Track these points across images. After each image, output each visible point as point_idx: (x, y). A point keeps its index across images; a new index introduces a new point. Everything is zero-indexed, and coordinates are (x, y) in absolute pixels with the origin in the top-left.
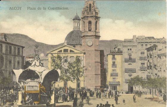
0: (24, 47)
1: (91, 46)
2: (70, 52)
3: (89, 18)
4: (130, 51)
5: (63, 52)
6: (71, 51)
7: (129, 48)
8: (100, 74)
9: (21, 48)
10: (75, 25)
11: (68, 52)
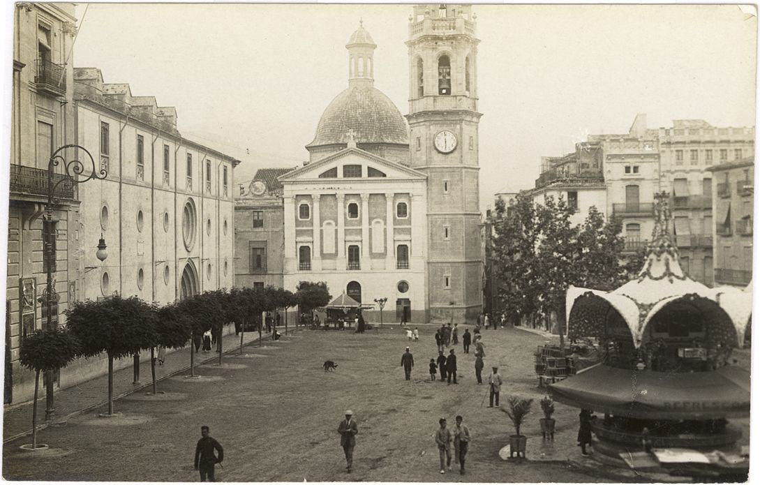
0: (239, 162)
1: (452, 152)
2: (369, 175)
3: (440, 43)
4: (632, 175)
5: (340, 173)
6: (372, 172)
7: (632, 162)
8: (42, 260)
9: (229, 166)
10: (365, 66)
11: (360, 176)
